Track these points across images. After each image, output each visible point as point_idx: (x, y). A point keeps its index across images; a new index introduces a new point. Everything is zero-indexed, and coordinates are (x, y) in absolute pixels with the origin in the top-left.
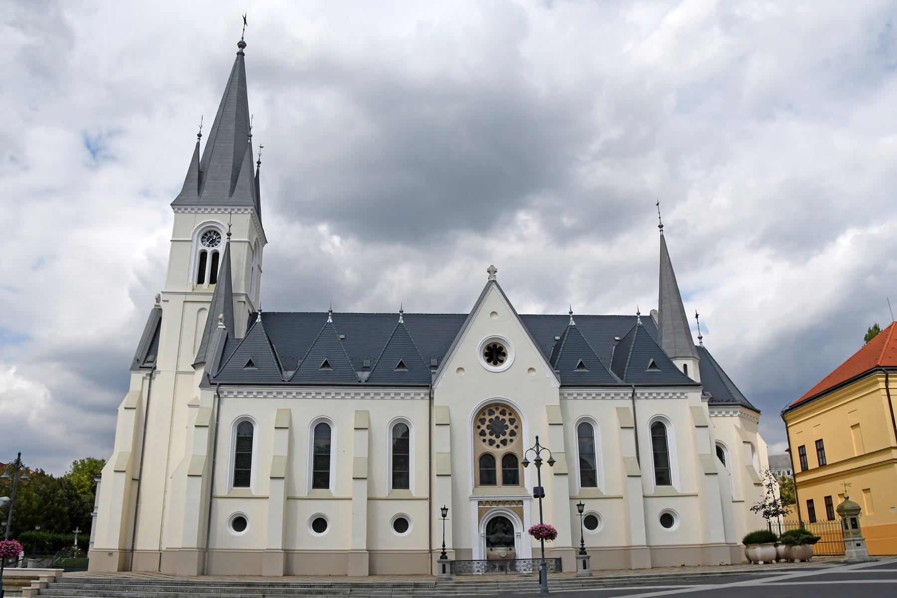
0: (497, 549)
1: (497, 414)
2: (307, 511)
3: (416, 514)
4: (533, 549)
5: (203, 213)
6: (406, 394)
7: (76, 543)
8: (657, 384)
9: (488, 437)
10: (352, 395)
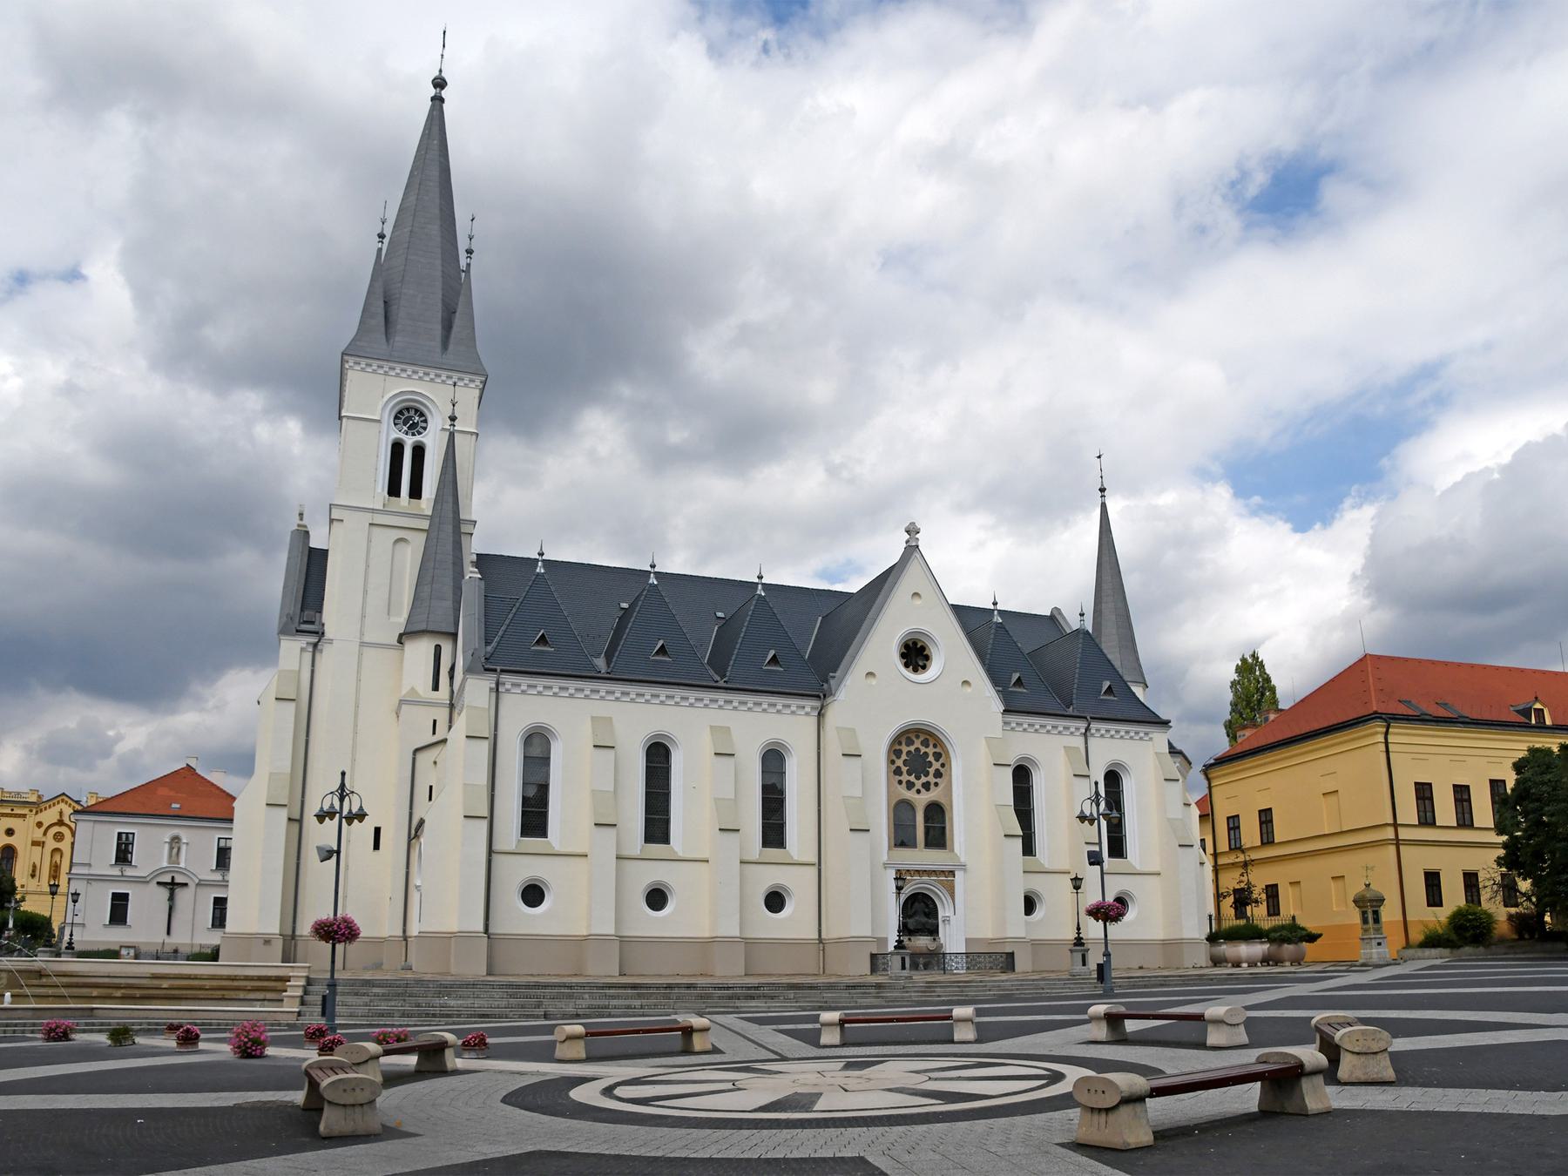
0: (919, 939)
1: (917, 744)
2: (514, 874)
3: (799, 886)
4: (966, 939)
5: (397, 375)
6: (785, 706)
7: (11, 925)
8: (1119, 717)
9: (905, 777)
10: (705, 702)
